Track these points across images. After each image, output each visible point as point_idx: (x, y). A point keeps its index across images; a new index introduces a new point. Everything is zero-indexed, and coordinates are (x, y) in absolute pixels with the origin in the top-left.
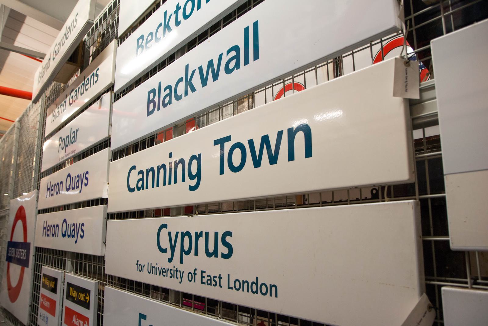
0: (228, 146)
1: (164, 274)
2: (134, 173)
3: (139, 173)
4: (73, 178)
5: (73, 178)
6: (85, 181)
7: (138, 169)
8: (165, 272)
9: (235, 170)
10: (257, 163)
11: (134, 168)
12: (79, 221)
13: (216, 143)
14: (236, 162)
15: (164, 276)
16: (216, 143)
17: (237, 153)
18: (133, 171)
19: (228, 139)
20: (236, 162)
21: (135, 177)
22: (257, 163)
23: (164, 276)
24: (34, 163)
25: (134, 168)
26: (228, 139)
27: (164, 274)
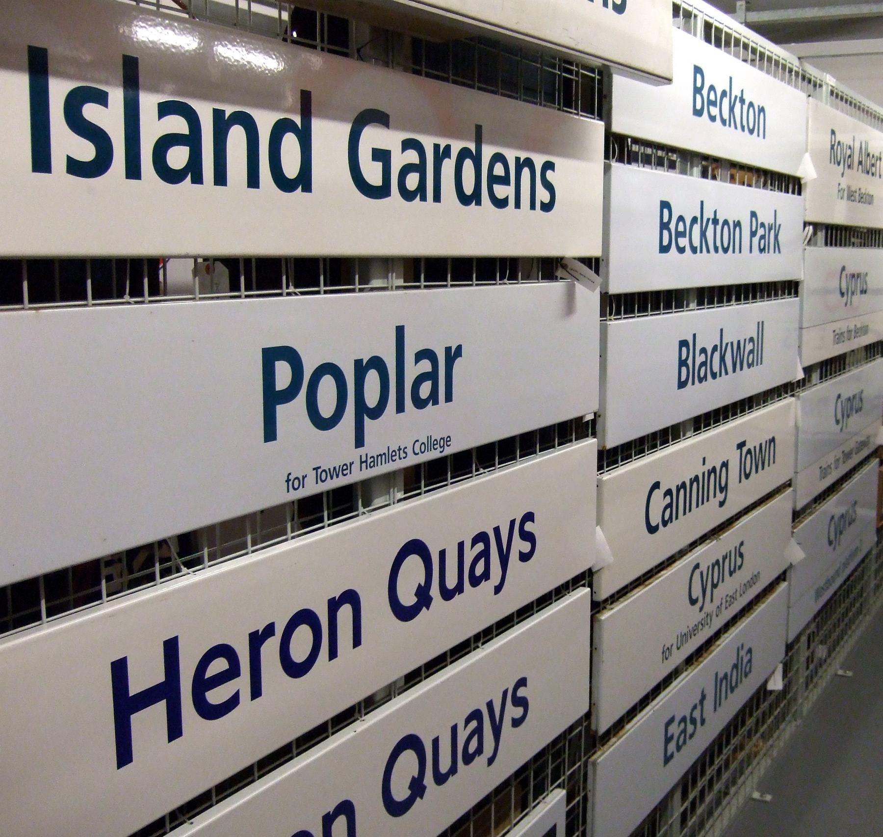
0: (320, 471)
1: (501, 191)
2: (658, 494)
3: (665, 495)
4: (442, 554)
5: (442, 554)
6: (520, 545)
7: (663, 488)
8: (505, 180)
9: (323, 481)
10: (332, 478)
11: (656, 485)
12: (837, 346)
13: (314, 469)
14: (323, 478)
15: (501, 203)
16: (314, 469)
17: (324, 474)
18: (656, 491)
19: (319, 468)
20: (323, 478)
21: (659, 501)
22: (332, 478)
23: (501, 203)
24: (782, 705)
25: (656, 485)
26: (319, 468)
27: (501, 191)
